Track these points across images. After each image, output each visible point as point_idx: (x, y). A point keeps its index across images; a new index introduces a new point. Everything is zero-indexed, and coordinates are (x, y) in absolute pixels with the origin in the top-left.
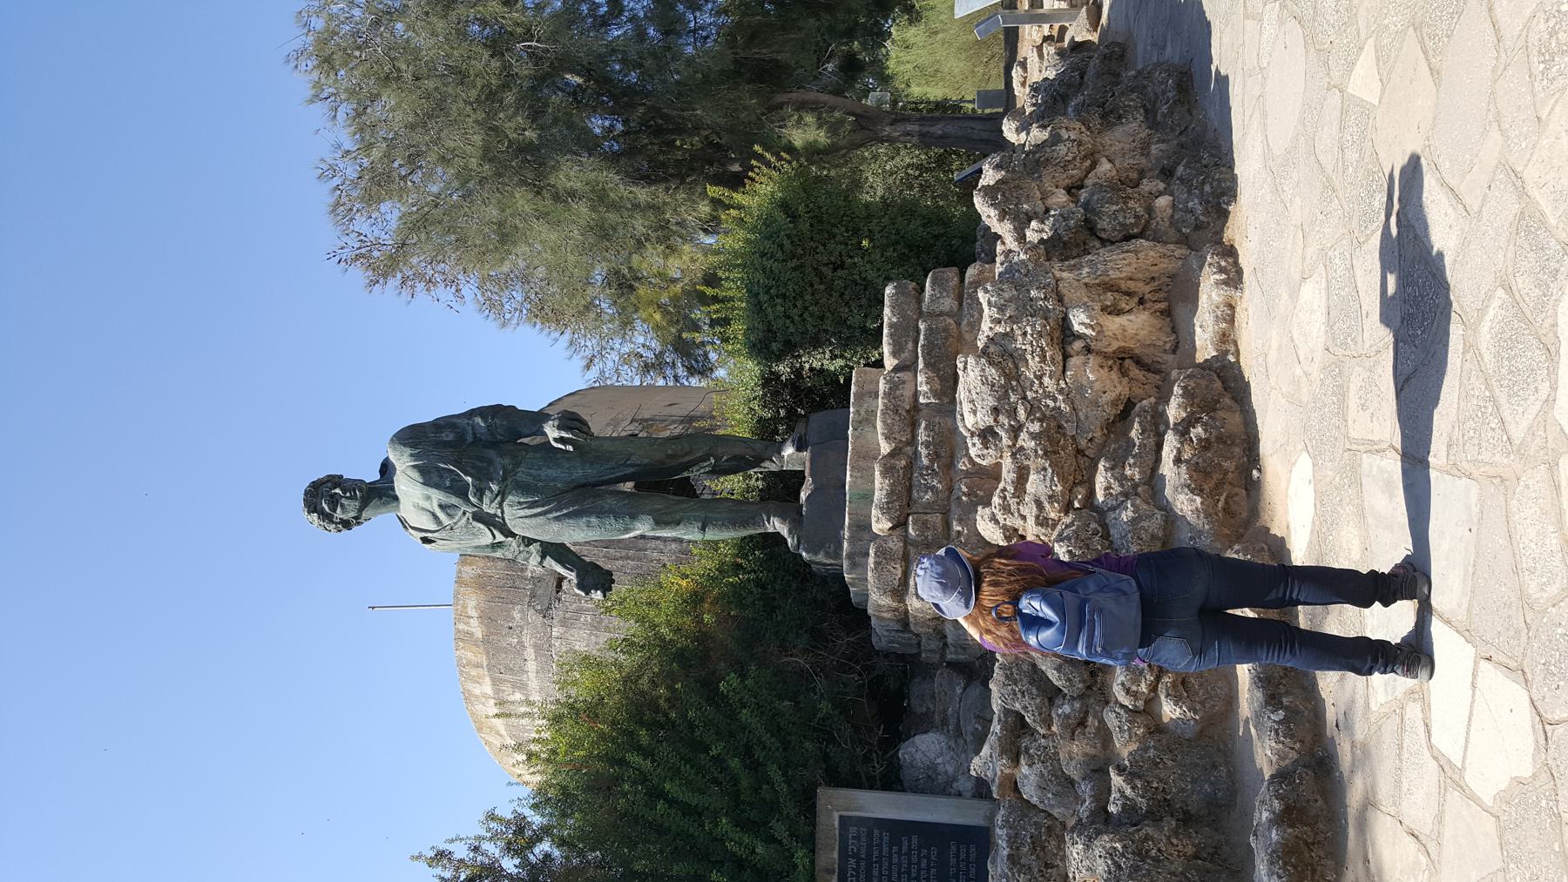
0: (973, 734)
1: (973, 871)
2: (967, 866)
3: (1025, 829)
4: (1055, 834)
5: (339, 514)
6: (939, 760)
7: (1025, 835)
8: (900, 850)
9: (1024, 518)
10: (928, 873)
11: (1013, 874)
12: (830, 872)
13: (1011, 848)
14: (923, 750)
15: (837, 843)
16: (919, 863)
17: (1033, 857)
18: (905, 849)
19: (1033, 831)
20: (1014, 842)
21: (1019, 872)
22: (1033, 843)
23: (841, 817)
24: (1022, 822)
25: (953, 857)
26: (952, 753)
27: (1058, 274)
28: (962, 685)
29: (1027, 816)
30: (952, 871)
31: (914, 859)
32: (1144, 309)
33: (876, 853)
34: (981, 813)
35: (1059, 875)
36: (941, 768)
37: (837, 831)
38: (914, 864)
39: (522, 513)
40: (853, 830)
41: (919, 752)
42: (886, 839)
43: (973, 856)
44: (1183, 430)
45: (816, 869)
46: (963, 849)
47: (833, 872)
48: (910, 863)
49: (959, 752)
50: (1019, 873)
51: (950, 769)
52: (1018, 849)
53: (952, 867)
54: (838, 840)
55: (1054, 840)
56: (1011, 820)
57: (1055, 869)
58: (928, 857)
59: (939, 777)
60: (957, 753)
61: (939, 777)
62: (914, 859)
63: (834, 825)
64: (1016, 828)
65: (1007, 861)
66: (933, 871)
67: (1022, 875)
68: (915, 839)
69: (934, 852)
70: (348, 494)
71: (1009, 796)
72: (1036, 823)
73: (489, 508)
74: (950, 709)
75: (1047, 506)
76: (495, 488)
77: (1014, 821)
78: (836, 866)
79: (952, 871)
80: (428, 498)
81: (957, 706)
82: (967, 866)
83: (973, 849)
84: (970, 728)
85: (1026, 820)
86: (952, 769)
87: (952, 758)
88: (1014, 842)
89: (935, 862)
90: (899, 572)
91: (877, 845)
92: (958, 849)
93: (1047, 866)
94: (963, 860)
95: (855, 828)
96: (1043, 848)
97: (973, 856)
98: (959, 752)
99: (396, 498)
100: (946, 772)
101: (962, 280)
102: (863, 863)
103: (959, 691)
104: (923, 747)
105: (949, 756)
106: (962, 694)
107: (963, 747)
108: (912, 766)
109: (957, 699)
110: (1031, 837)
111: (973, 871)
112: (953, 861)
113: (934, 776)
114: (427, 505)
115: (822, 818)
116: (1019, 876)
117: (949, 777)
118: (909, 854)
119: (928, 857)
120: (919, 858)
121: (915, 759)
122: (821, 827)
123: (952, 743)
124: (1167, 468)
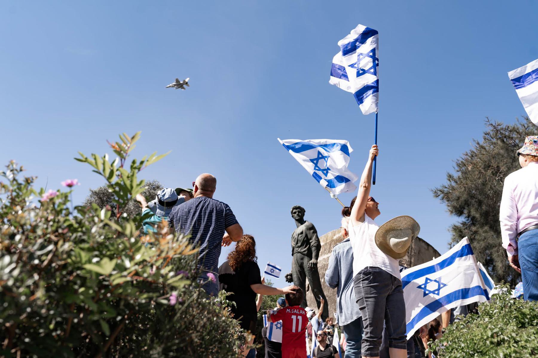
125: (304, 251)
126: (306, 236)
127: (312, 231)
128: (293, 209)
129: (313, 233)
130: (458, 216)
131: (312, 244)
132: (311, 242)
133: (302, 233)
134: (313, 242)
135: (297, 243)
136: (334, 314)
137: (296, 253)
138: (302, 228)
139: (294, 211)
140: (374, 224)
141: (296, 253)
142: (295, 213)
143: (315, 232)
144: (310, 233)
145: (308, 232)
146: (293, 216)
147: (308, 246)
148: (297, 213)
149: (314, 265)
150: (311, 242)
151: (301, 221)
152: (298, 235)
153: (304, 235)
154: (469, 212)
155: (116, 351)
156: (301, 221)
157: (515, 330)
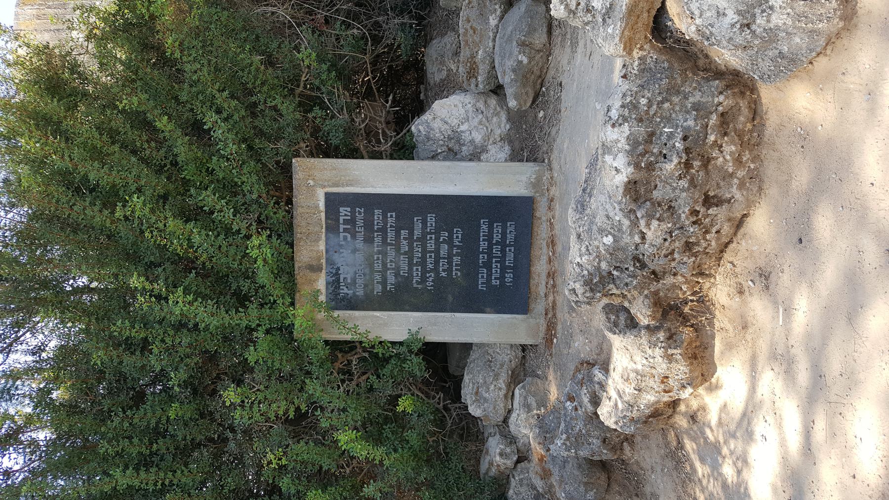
0: (514, 71)
1: (510, 256)
2: (503, 251)
3: (668, 120)
4: (735, 131)
6: (463, 128)
7: (671, 136)
8: (411, 233)
10: (450, 263)
11: (635, 223)
12: (315, 269)
13: (637, 166)
14: (443, 116)
15: (324, 230)
16: (437, 251)
17: (684, 183)
18: (417, 233)
19: (691, 123)
20: (643, 155)
21: (650, 217)
22: (687, 151)
23: (327, 195)
24: (667, 105)
25: (484, 240)
26: (480, 116)
28: (498, 13)
29: (678, 92)
30: (483, 258)
31: (431, 246)
34: (524, 178)
35: (729, 220)
36: (466, 137)
37: (323, 215)
38: (431, 252)
40: (344, 211)
41: (438, 120)
42: (391, 221)
43: (510, 238)
45: (296, 266)
46: (497, 228)
47: (319, 269)
48: (424, 251)
49: (489, 115)
50: (650, 217)
51: (478, 137)
52: (650, 167)
53: (483, 253)
54: (324, 226)
55: (732, 142)
56: (644, 101)
57: (725, 206)
58: (450, 241)
59: (464, 148)
60: (487, 118)
61: (464, 148)
62: (431, 246)
63: (317, 207)
64: (651, 120)
65: (625, 195)
66: (456, 260)
67: (655, 223)
68: (431, 220)
69: (458, 233)
71: (641, 49)
72: (697, 107)
74: (480, 52)
77: (650, 104)
78: (323, 261)
79: (483, 258)
81: (491, 44)
82: (503, 251)
83: (511, 227)
84: (510, 63)
85: (676, 99)
86: (480, 137)
87: (480, 123)
88: (643, 155)
89: (458, 247)
91: (379, 230)
92: (491, 228)
93: (708, 201)
94: (497, 243)
95: (349, 209)
96: (706, 162)
97: (510, 238)
98: (489, 115)
100: (472, 141)
103: (493, 21)
105: (477, 120)
106: (497, 26)
107: (496, 109)
108: (428, 139)
109: (491, 34)
110: (685, 138)
111: (510, 256)
112: (483, 245)
113: (456, 148)
115: (300, 198)
116: (648, 225)
117: (476, 147)
118: (423, 239)
119: (450, 241)
120: (438, 243)
121: (432, 129)
122: (300, 210)
123: (481, 105)
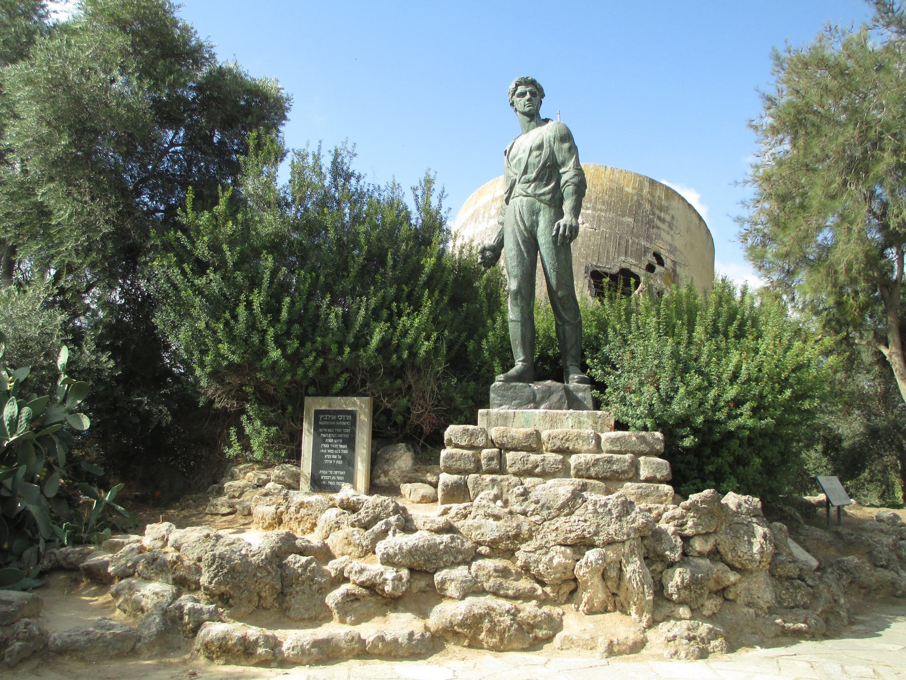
5: (515, 99)
9: (475, 518)
16: (335, 454)
27: (627, 543)
30: (331, 472)
32: (608, 596)
33: (339, 430)
39: (517, 208)
44: (514, 613)
69: (340, 462)
70: (239, 276)
73: (518, 189)
75: (477, 532)
76: (530, 191)
80: (524, 151)
90: (463, 444)
99: (528, 131)
101: (661, 482)
102: (333, 423)
104: (404, 457)
112: (336, 472)
114: (521, 150)
124: (489, 601)
125: (544, 194)
126: (552, 154)
127: (566, 145)
128: (517, 86)
129: (570, 149)
130: (756, 266)
131: (564, 178)
132: (564, 173)
133: (540, 147)
134: (567, 174)
135: (525, 172)
136: (561, 613)
137: (521, 195)
138: (545, 133)
139: (521, 89)
140: (412, 611)
141: (521, 197)
142: (523, 95)
143: (573, 150)
144: (560, 150)
145: (556, 147)
146: (512, 104)
147: (552, 185)
148: (528, 96)
149: (571, 232)
150: (564, 173)
151: (534, 117)
152: (531, 151)
153: (546, 151)
154: (832, 444)
155: (56, 326)
156: (534, 117)
157: (790, 297)
